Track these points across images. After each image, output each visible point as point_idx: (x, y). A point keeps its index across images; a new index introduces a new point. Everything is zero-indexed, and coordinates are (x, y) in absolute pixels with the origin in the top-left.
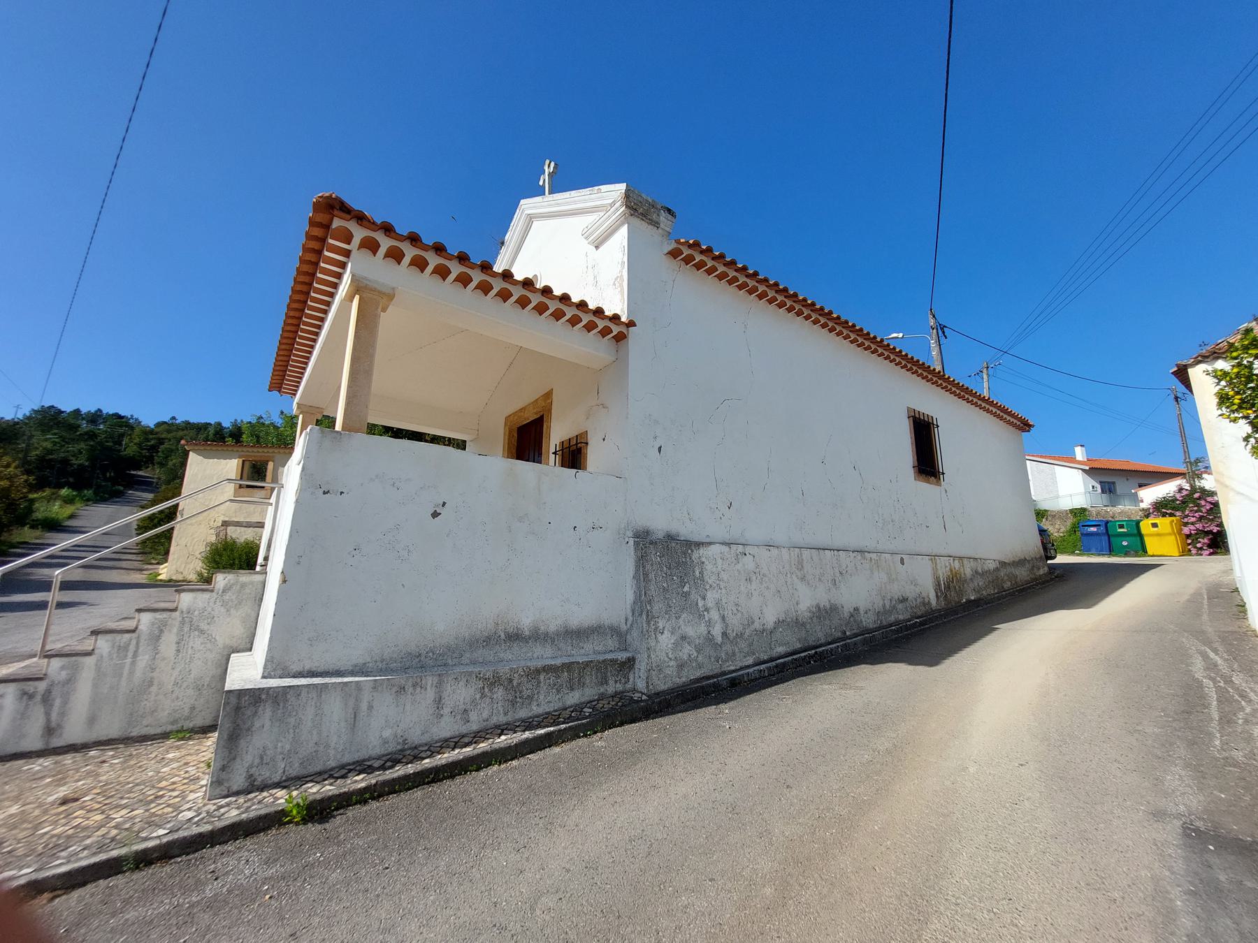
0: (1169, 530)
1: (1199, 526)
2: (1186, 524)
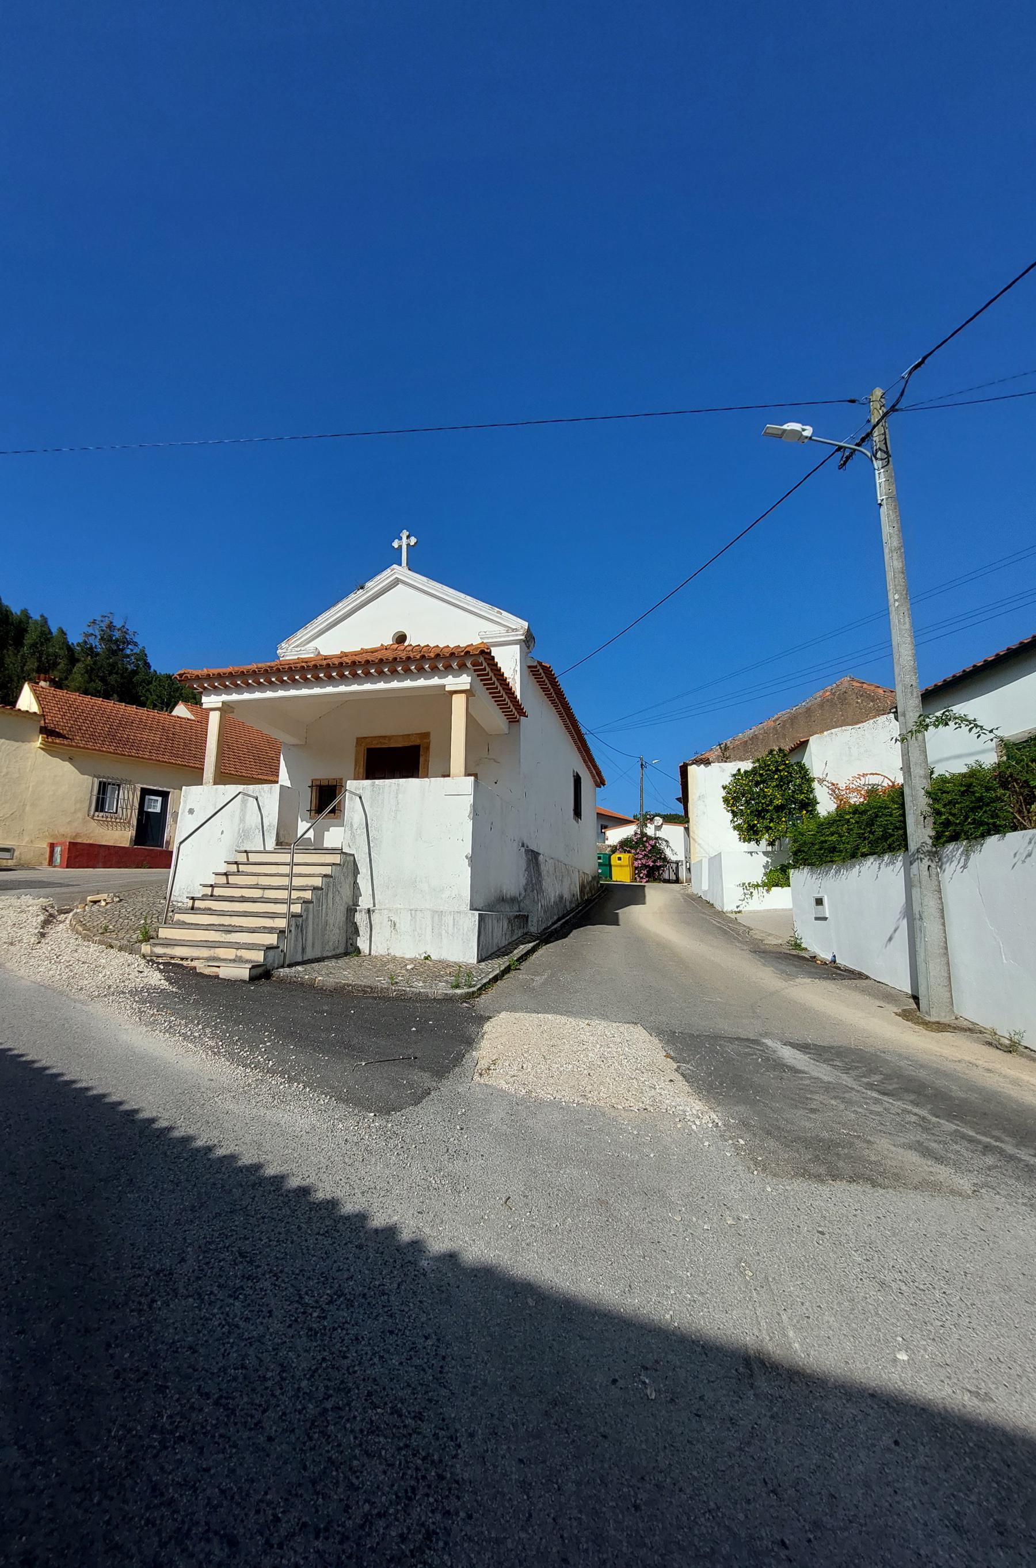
0: (627, 863)
1: (644, 861)
2: (636, 859)
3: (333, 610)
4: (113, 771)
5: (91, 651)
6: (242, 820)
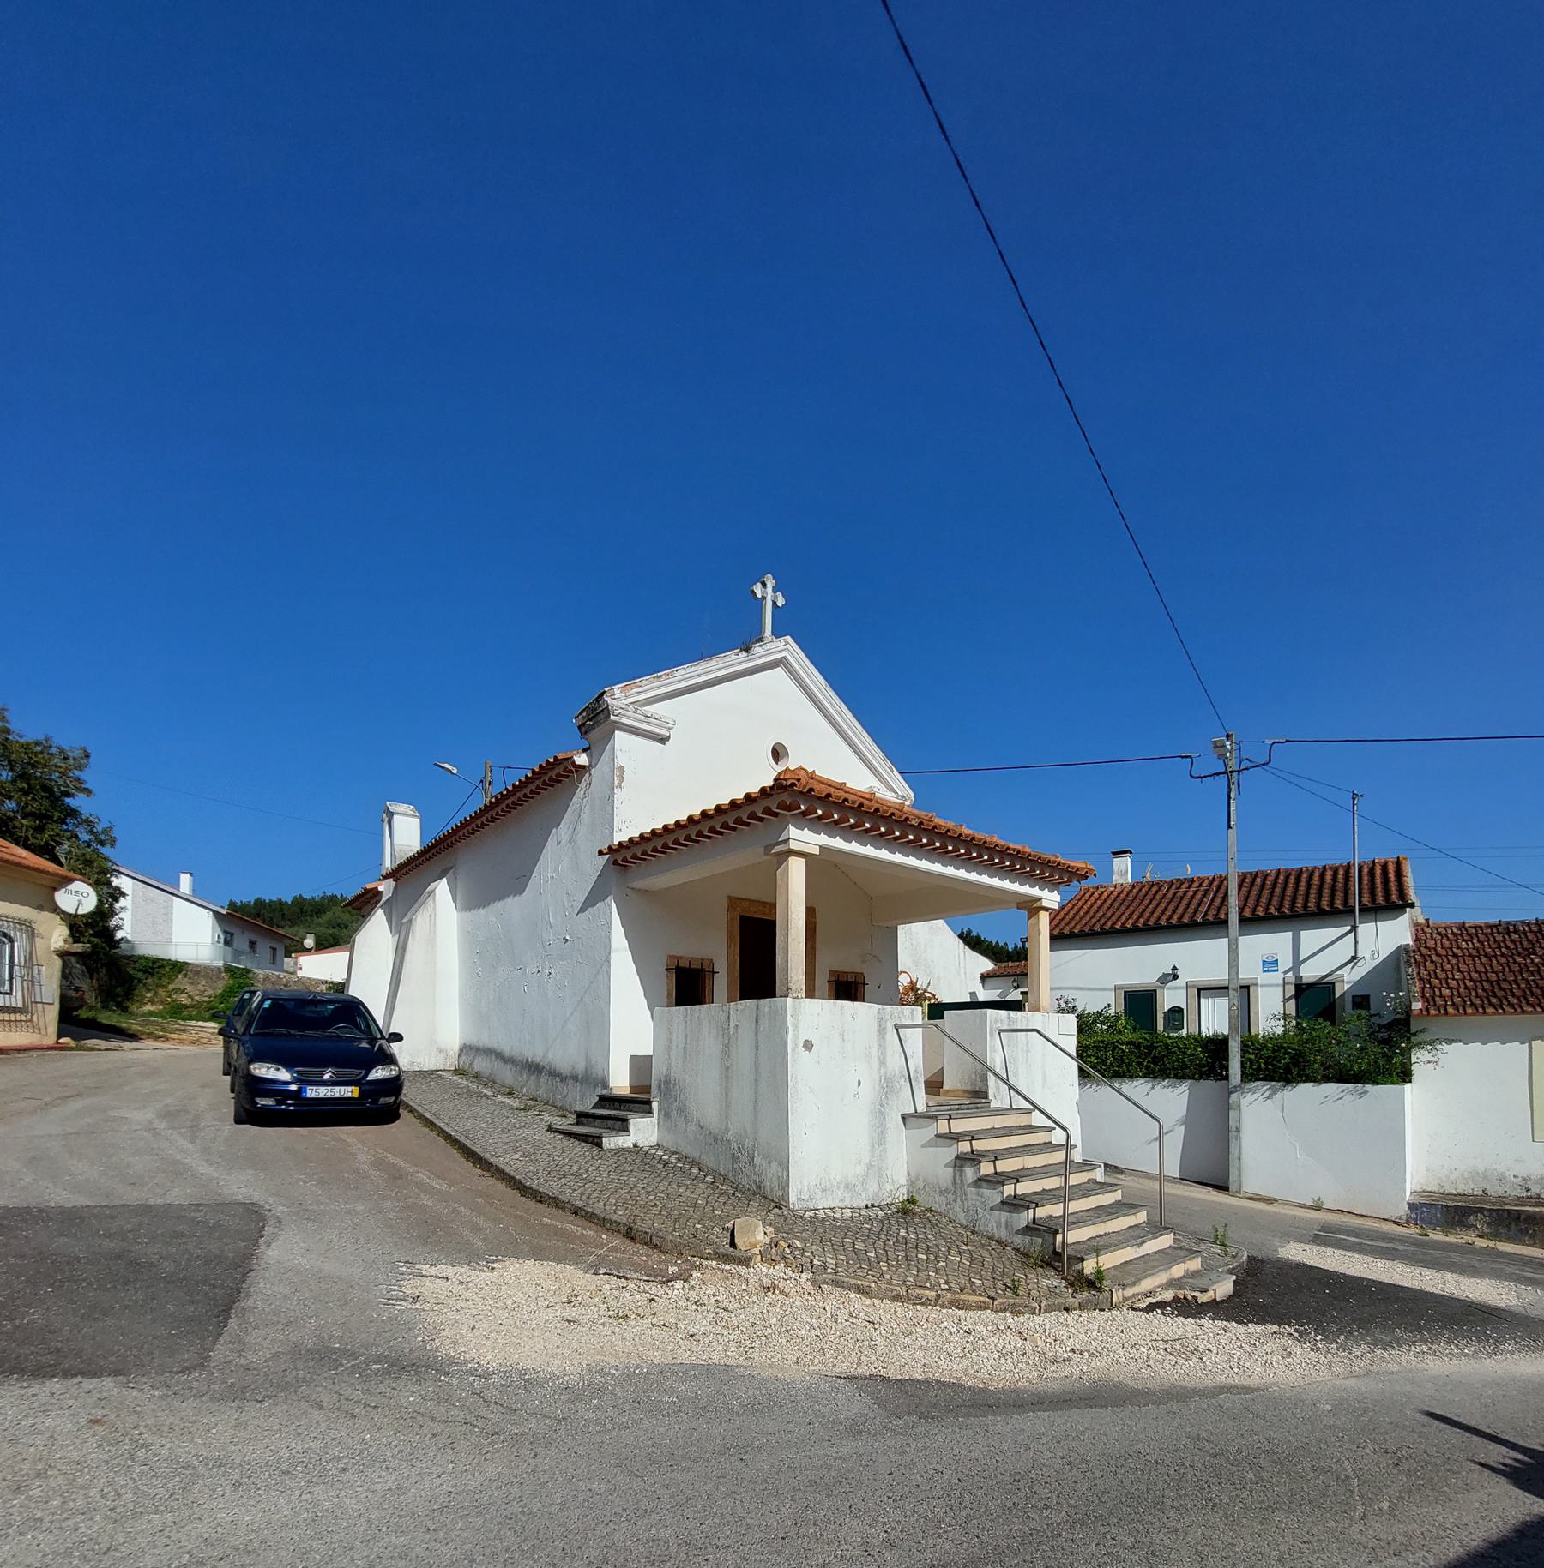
3: (713, 663)
6: (882, 1063)
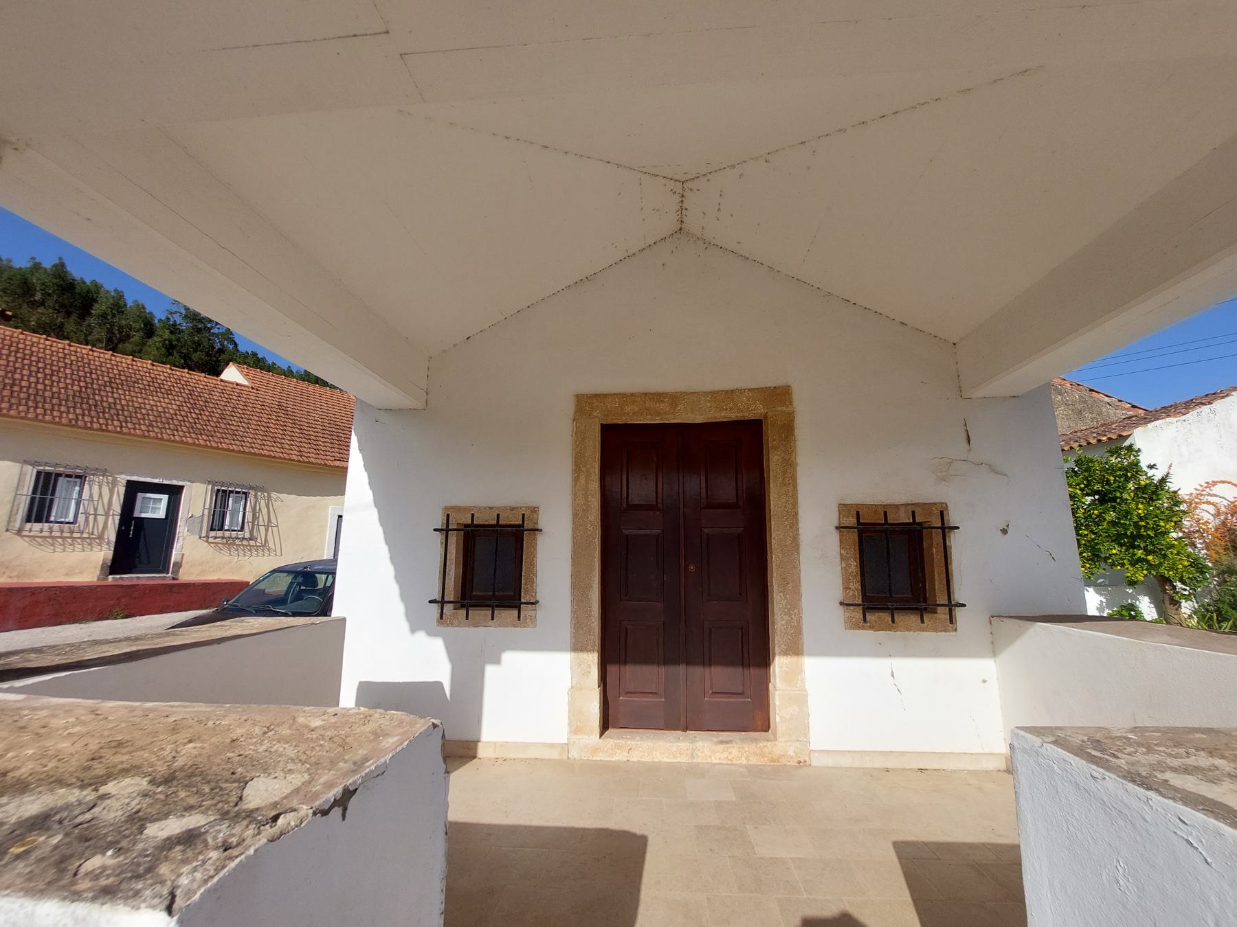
4: (62, 453)
5: (174, 329)
